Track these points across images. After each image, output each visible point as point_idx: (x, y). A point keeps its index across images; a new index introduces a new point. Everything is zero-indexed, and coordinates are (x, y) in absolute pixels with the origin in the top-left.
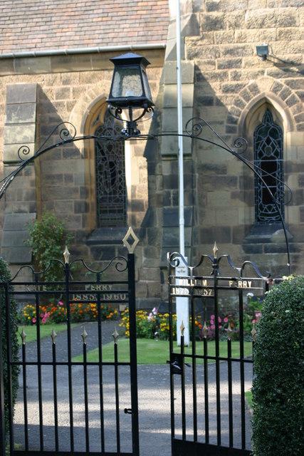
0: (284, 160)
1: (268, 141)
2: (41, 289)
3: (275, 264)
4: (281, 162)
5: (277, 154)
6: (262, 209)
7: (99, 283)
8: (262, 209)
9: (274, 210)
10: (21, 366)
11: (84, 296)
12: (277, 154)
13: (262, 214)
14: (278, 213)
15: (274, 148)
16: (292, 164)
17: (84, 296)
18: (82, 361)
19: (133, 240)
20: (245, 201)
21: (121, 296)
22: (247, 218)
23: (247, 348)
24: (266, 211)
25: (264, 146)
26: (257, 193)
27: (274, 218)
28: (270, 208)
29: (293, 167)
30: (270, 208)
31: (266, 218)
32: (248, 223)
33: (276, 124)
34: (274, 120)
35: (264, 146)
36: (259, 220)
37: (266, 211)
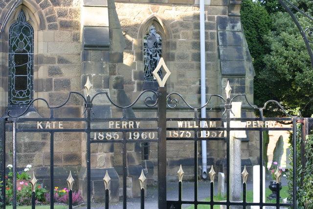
0: (35, 53)
1: (21, 37)
2: (57, 125)
3: (27, 140)
4: (32, 56)
5: (28, 48)
6: (14, 94)
7: (52, 131)
8: (14, 94)
9: (24, 96)
10: (264, 201)
11: (107, 134)
12: (28, 48)
13: (14, 99)
14: (28, 98)
15: (26, 43)
16: (44, 57)
17: (107, 134)
18: (209, 201)
19: (159, 72)
20: (2, 87)
21: (150, 134)
22: (4, 100)
23: (248, 198)
24: (18, 95)
25: (18, 41)
26: (10, 80)
27: (24, 102)
28: (21, 93)
29: (45, 59)
30: (21, 93)
31: (18, 102)
32: (4, 105)
33: (28, 23)
34: (27, 20)
35: (18, 41)
36: (12, 104)
37: (18, 95)
